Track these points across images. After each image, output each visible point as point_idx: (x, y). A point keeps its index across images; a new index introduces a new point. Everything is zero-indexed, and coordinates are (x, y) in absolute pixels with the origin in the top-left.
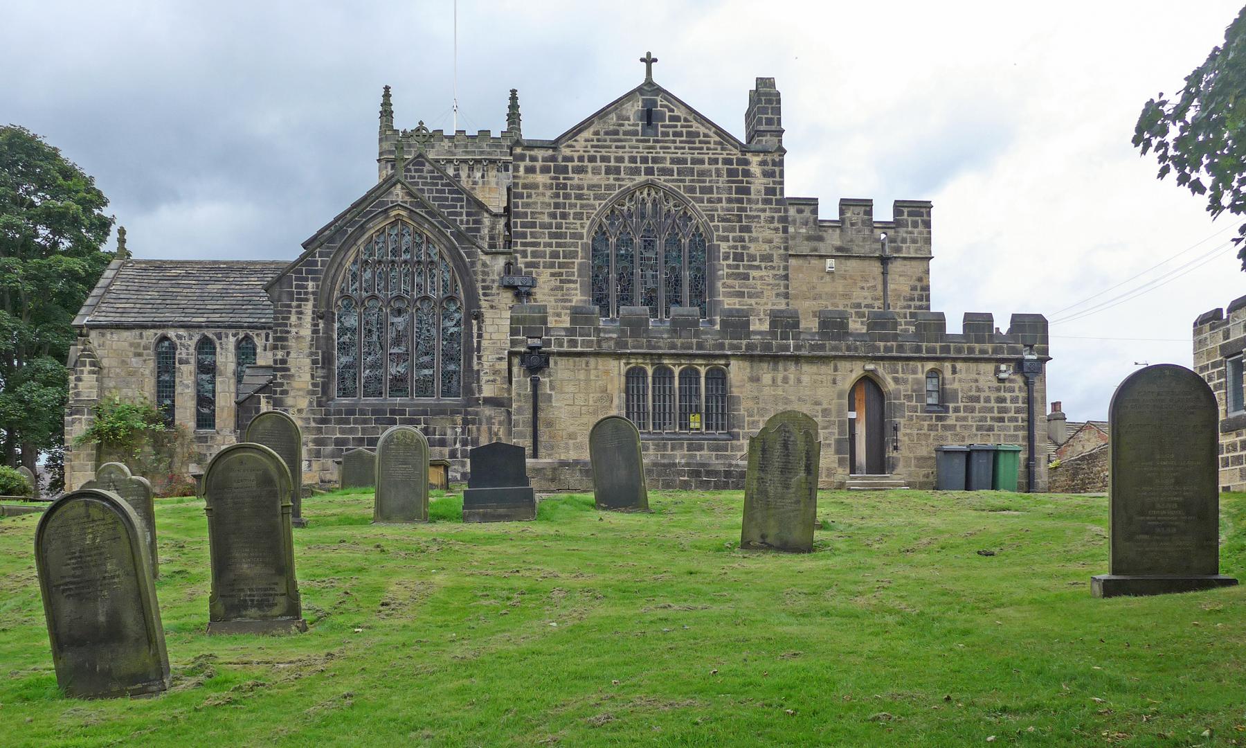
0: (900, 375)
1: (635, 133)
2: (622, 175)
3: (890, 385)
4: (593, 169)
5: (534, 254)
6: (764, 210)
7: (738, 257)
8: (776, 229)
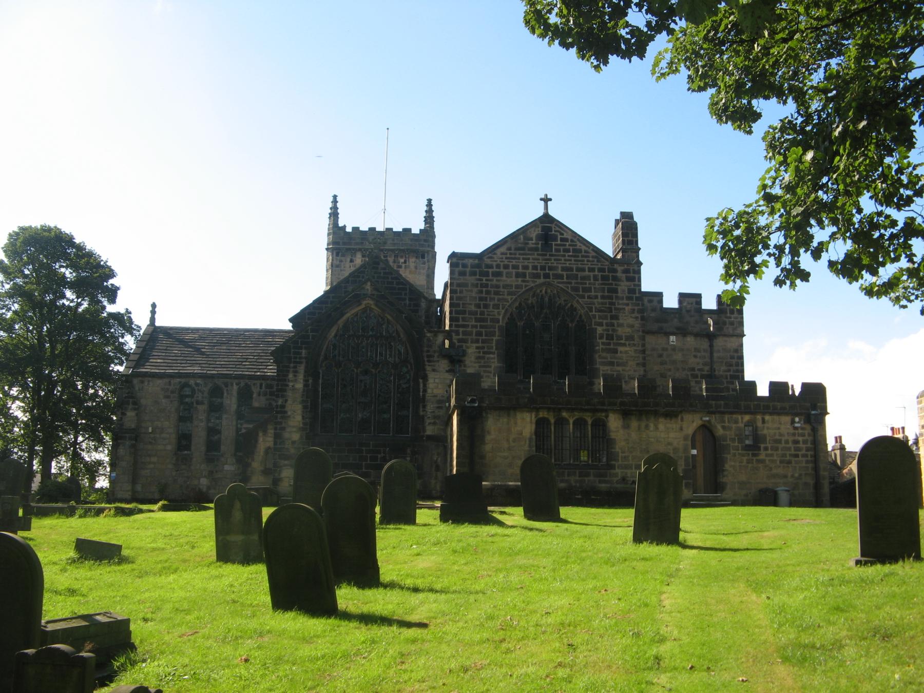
0: (727, 424)
1: (536, 249)
2: (528, 278)
3: (720, 431)
4: (507, 273)
5: (464, 333)
6: (628, 305)
7: (610, 337)
8: (637, 318)
